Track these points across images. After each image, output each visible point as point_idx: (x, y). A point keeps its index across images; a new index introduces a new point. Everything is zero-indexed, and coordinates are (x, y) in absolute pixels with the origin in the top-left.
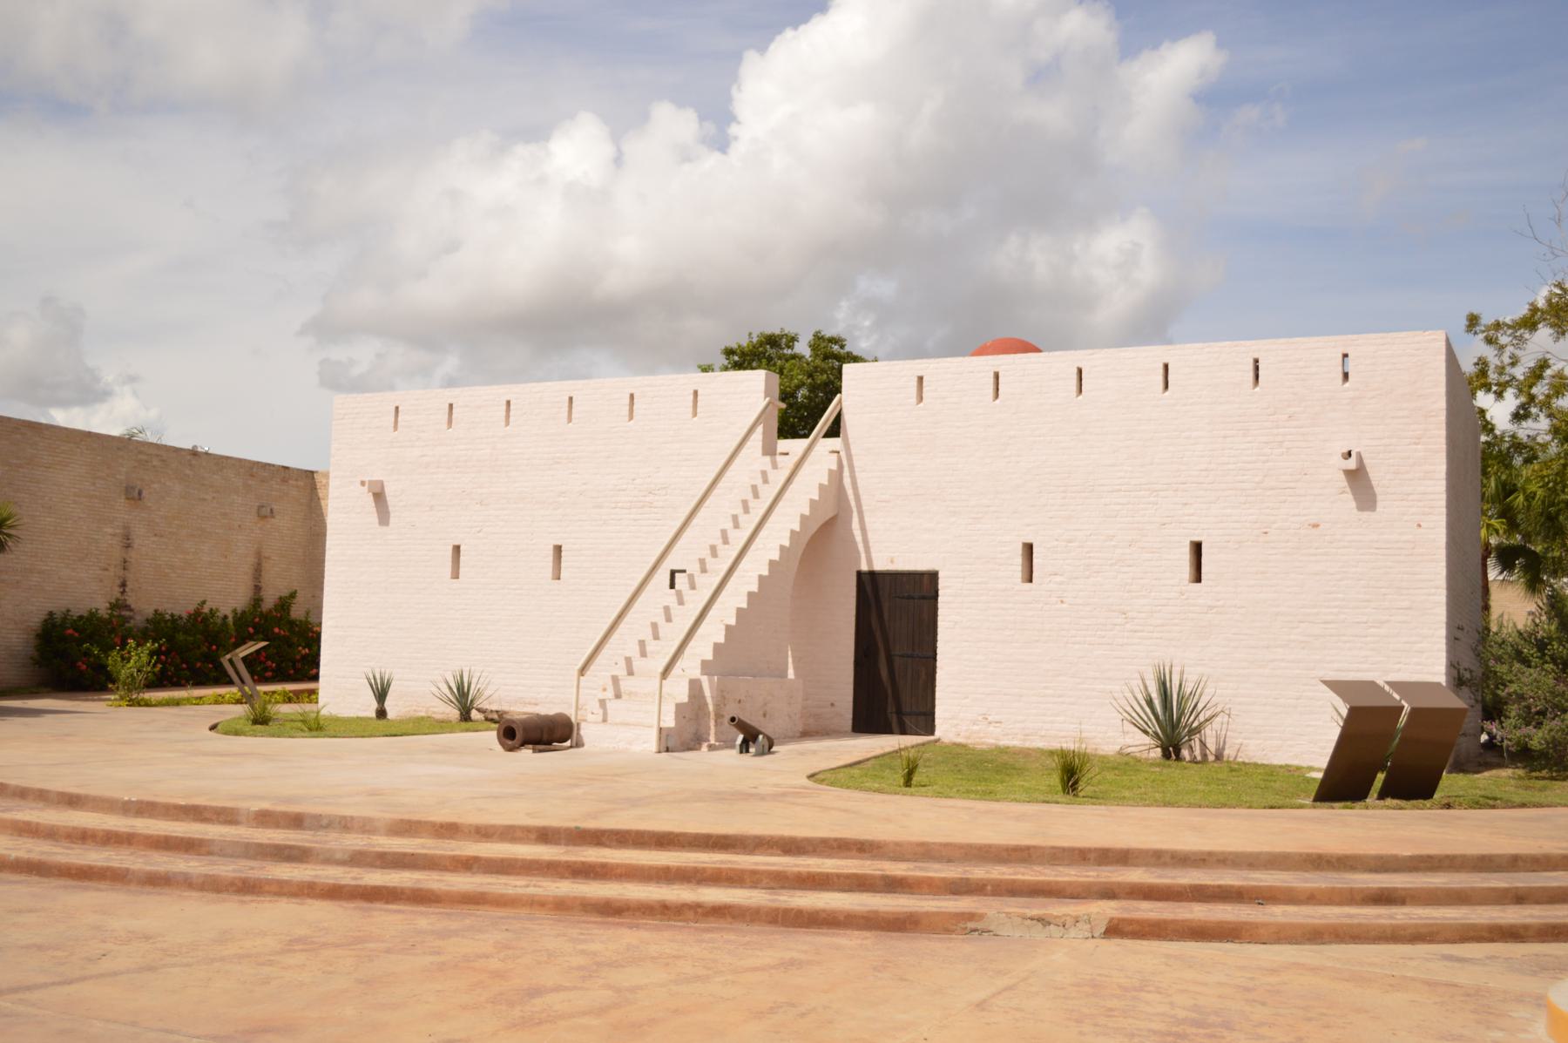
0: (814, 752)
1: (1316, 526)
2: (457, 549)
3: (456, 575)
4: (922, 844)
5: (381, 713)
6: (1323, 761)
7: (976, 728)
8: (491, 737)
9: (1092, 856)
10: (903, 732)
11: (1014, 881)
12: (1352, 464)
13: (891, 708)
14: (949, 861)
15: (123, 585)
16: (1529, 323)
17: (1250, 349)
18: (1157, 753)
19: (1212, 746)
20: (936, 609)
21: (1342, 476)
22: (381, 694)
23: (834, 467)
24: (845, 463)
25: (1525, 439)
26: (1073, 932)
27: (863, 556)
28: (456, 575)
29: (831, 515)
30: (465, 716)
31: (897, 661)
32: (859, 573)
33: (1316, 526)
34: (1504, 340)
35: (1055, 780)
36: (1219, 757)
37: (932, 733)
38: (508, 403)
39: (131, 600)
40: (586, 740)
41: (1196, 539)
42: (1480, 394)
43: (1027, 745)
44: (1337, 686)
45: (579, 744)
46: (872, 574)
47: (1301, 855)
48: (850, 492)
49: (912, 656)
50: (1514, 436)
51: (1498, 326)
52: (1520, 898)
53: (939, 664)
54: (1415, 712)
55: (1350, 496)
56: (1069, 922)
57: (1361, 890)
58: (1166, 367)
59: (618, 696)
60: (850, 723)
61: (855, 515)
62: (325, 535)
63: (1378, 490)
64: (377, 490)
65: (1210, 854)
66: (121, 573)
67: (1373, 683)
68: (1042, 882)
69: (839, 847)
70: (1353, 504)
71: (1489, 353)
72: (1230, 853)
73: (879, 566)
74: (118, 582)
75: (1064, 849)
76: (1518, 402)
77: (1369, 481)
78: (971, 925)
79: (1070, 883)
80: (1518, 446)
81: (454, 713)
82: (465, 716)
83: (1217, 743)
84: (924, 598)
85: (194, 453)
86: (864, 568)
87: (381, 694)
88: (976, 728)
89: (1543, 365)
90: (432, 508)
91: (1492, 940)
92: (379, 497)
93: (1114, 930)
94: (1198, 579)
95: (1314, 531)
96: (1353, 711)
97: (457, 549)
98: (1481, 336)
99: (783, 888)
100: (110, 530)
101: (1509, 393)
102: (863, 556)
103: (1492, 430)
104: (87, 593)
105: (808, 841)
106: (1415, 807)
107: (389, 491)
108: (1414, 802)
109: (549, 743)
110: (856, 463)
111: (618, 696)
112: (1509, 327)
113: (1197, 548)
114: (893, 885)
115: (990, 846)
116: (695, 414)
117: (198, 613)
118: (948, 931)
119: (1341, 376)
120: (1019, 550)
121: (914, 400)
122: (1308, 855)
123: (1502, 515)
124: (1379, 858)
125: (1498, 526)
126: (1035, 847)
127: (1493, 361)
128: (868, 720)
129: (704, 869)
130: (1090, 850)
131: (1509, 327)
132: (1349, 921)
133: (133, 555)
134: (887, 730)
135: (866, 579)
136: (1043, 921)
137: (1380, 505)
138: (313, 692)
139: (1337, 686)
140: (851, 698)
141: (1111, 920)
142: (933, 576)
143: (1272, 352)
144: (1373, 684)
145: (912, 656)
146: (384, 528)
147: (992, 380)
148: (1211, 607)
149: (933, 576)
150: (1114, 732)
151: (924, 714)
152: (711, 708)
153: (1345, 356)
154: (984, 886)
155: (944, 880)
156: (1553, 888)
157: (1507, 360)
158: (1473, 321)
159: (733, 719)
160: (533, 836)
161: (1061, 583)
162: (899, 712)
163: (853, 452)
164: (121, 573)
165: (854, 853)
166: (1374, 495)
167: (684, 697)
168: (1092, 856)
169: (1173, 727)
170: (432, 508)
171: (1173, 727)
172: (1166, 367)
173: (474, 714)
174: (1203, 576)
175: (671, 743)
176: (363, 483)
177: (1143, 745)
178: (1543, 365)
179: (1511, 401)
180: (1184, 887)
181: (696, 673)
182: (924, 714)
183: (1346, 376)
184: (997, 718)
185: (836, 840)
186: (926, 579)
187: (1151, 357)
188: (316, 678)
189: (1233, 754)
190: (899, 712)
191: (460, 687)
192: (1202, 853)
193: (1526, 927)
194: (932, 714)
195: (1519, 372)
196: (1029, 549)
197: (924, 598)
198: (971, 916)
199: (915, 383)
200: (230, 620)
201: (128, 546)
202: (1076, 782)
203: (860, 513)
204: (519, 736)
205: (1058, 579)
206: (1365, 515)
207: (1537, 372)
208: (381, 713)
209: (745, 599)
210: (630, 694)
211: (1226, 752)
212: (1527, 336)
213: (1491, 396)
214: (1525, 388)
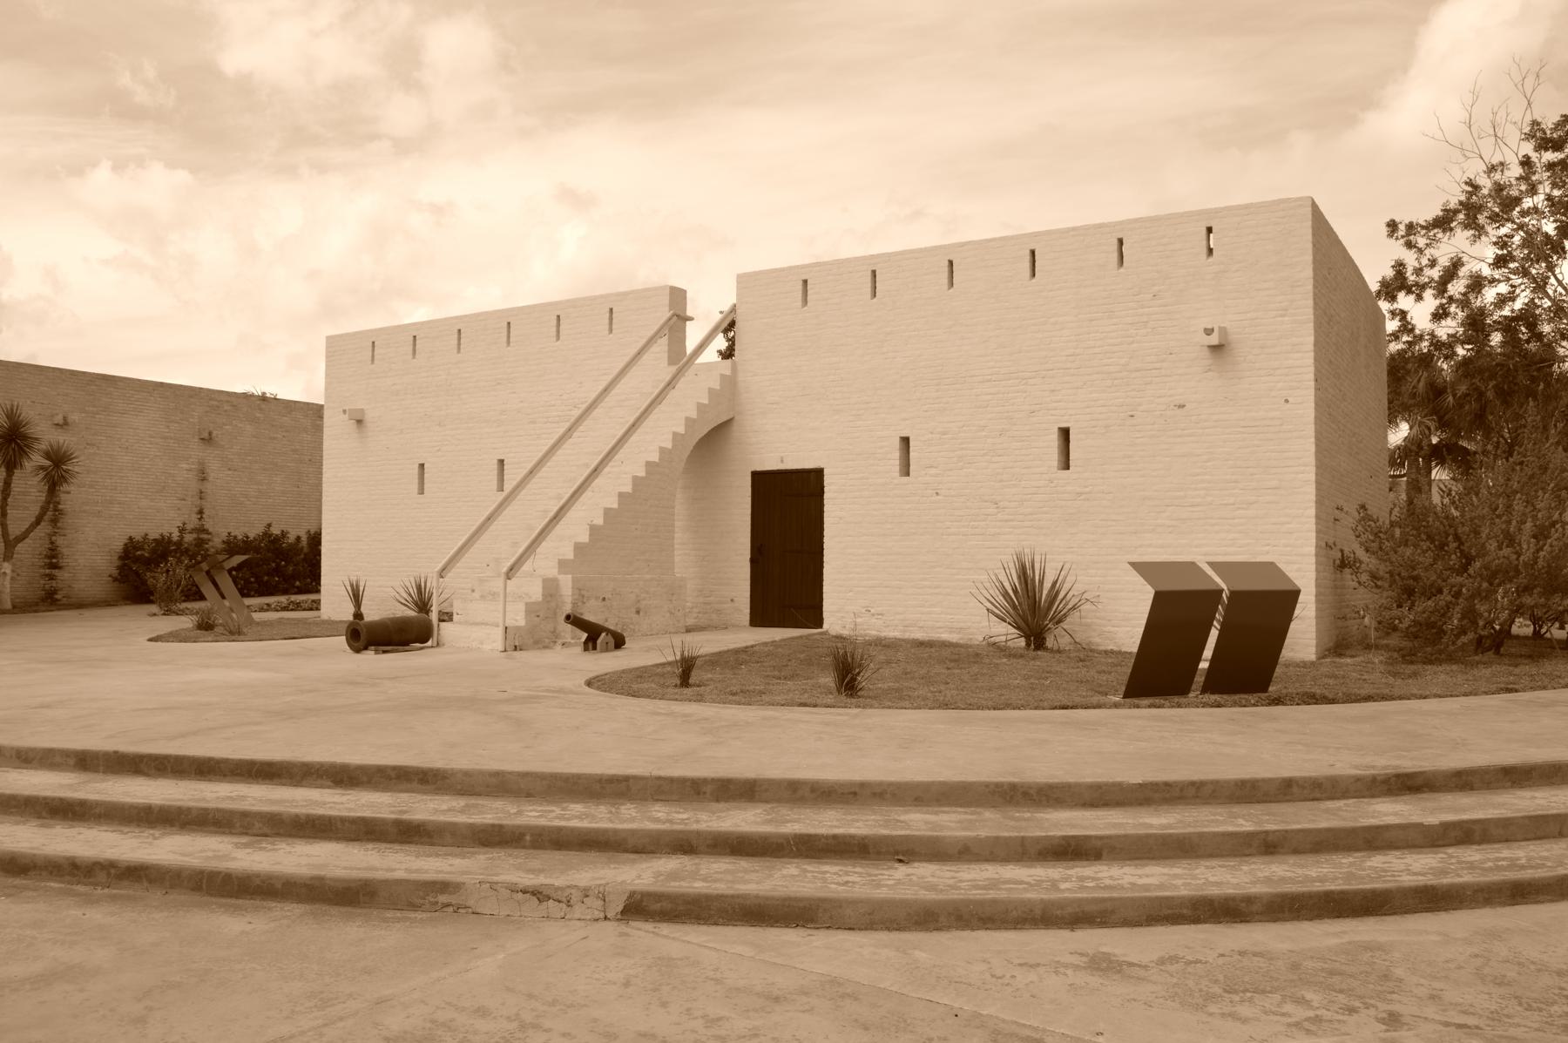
1: (1182, 406)
3: (421, 491)
4: (497, 774)
6: (1135, 650)
9: (708, 789)
11: (560, 829)
12: (1214, 340)
14: (529, 795)
15: (201, 512)
16: (1443, 222)
18: (1022, 642)
20: (822, 505)
23: (728, 373)
25: (1445, 337)
26: (578, 911)
28: (421, 491)
33: (1182, 406)
34: (1422, 242)
35: (828, 680)
42: (1401, 295)
44: (1142, 568)
47: (987, 785)
50: (1432, 334)
51: (1411, 227)
52: (1269, 845)
54: (1234, 595)
56: (576, 896)
57: (1038, 840)
58: (1033, 253)
65: (863, 785)
67: (1193, 563)
68: (597, 831)
69: (398, 777)
71: (1410, 259)
72: (891, 784)
75: (671, 780)
76: (1438, 302)
78: (443, 899)
79: (633, 832)
80: (1437, 344)
85: (263, 398)
89: (1456, 264)
91: (1196, 920)
93: (638, 908)
94: (1066, 466)
95: (1179, 412)
96: (1160, 598)
98: (1402, 241)
99: (278, 835)
101: (1428, 294)
103: (1412, 330)
104: (161, 517)
105: (363, 769)
106: (1235, 704)
108: (1236, 697)
109: (406, 643)
112: (1423, 227)
113: (1065, 433)
114: (408, 833)
115: (579, 776)
117: (266, 534)
118: (414, 907)
119: (1205, 250)
120: (897, 443)
121: (800, 304)
122: (997, 785)
123: (1434, 412)
124: (1097, 787)
125: (1429, 423)
126: (636, 778)
127: (1410, 259)
129: (189, 809)
130: (705, 781)
131: (1423, 227)
132: (992, 894)
133: (208, 487)
136: (539, 894)
138: (318, 602)
139: (1142, 568)
141: (632, 894)
142: (819, 473)
144: (1192, 565)
147: (869, 278)
149: (819, 473)
150: (974, 619)
153: (1210, 230)
154: (522, 835)
155: (471, 826)
156: (1319, 831)
157: (1425, 262)
158: (1392, 226)
159: (568, 617)
160: (72, 762)
165: (415, 785)
167: (536, 592)
168: (708, 789)
169: (1034, 611)
171: (1034, 611)
172: (1033, 253)
175: (516, 643)
177: (1004, 632)
178: (1456, 264)
179: (1430, 302)
180: (786, 837)
181: (553, 572)
183: (1210, 251)
185: (394, 768)
188: (318, 591)
191: (419, 588)
192: (852, 784)
193: (1249, 900)
195: (1435, 273)
196: (906, 441)
198: (444, 887)
199: (800, 286)
200: (304, 539)
201: (204, 479)
202: (854, 679)
204: (363, 637)
205: (933, 471)
207: (1451, 272)
212: (1440, 235)
213: (1412, 297)
214: (1441, 287)
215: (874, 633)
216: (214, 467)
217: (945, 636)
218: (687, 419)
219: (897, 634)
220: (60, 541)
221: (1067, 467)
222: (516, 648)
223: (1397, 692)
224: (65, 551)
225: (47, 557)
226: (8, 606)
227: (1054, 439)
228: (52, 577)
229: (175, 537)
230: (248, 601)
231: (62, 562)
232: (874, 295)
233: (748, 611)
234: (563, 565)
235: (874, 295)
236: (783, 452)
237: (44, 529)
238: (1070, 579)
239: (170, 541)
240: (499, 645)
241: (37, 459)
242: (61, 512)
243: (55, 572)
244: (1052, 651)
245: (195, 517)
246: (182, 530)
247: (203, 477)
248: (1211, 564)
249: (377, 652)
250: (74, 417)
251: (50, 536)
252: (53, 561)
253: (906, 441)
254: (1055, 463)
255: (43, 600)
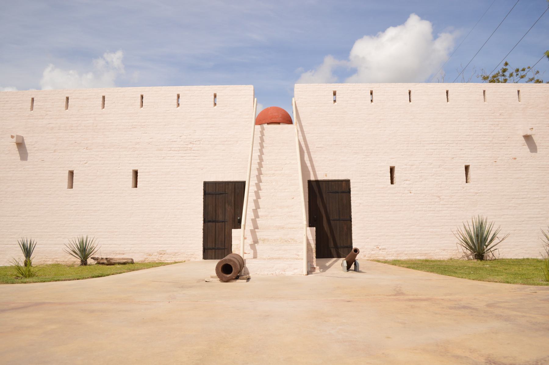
1: (515, 159)
2: (71, 173)
3: (71, 186)
5: (27, 263)
7: (373, 252)
13: (332, 244)
17: (139, 91)
21: (523, 139)
22: (28, 252)
28: (71, 186)
30: (84, 263)
33: (515, 159)
38: (104, 97)
43: (399, 258)
46: (317, 182)
55: (527, 147)
59: (255, 257)
62: (349, 192)
63: (537, 144)
64: (20, 141)
70: (528, 150)
73: (320, 177)
77: (533, 140)
81: (78, 261)
82: (84, 263)
84: (343, 192)
86: (312, 178)
87: (28, 252)
88: (373, 252)
90: (55, 151)
92: (20, 145)
95: (514, 161)
97: (71, 173)
107: (27, 142)
111: (255, 257)
135: (314, 185)
137: (538, 150)
142: (348, 182)
143: (149, 92)
145: (339, 220)
146: (24, 162)
148: (477, 193)
149: (348, 182)
150: (453, 249)
151: (347, 247)
161: (409, 184)
166: (536, 146)
169: (479, 245)
170: (55, 151)
171: (479, 245)
173: (90, 261)
176: (12, 137)
182: (347, 247)
184: (384, 247)
186: (344, 184)
187: (405, 87)
197: (343, 192)
199: (101, 99)
205: (408, 182)
206: (533, 154)
208: (27, 263)
210: (264, 240)
223: (105, 273)
227: (67, 175)
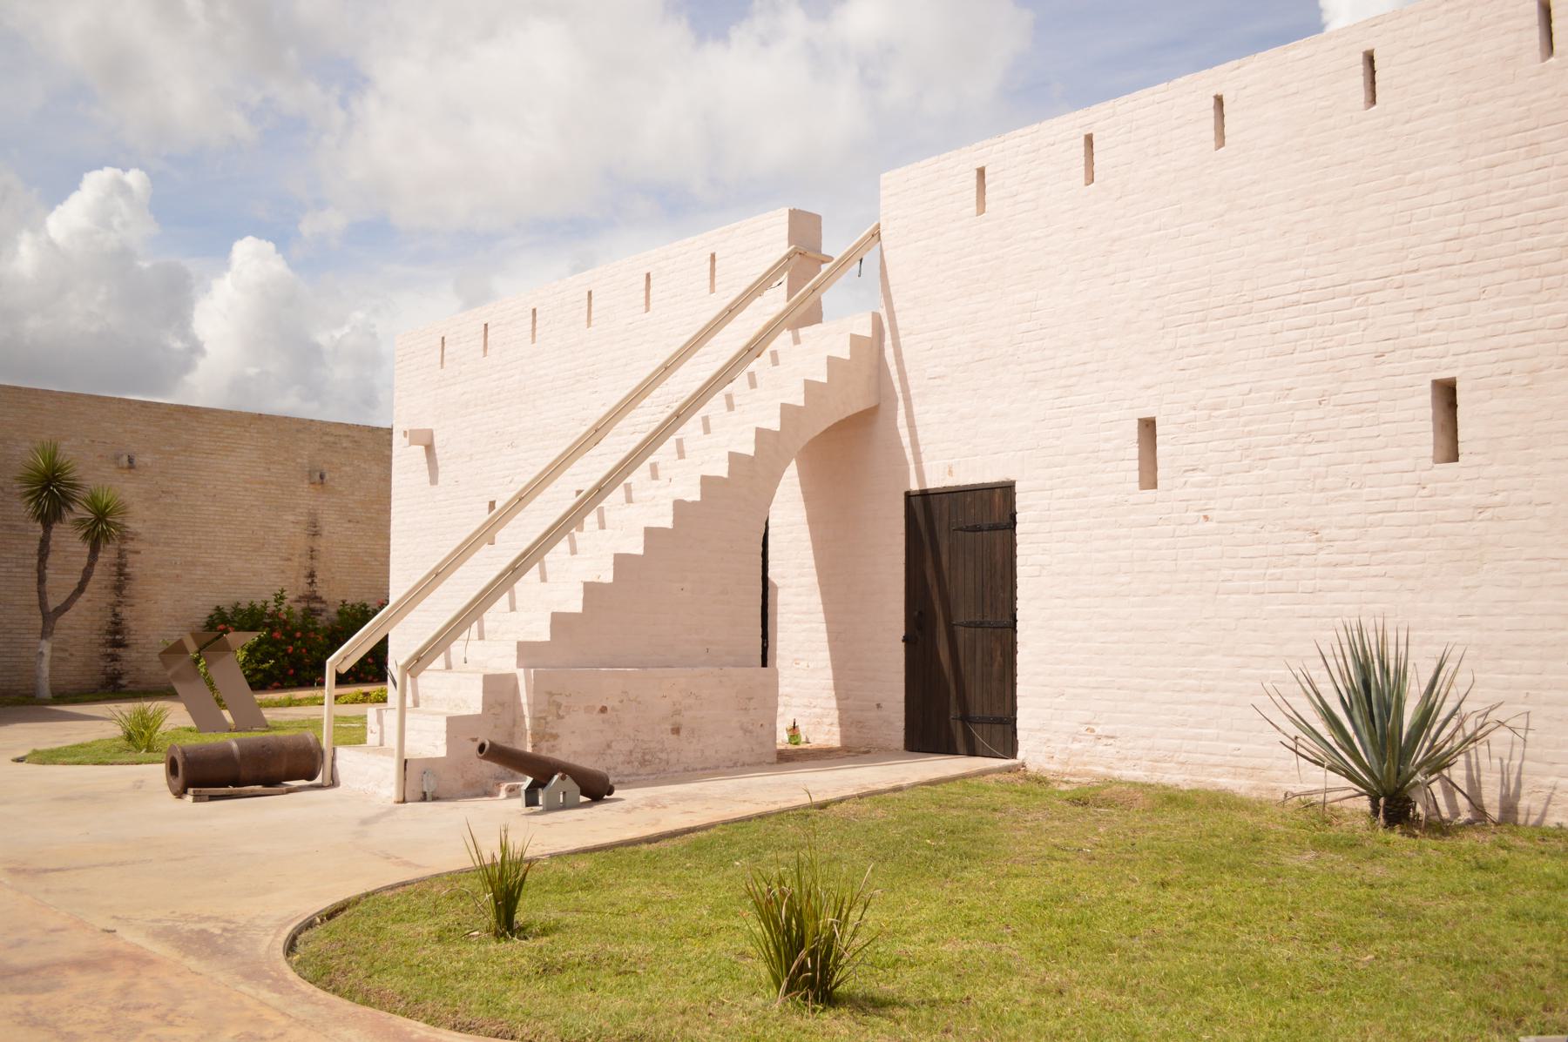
0: (693, 798)
8: (157, 772)
10: (972, 752)
13: (954, 713)
15: (312, 575)
19: (1491, 798)
24: (886, 325)
27: (912, 467)
29: (859, 406)
31: (963, 635)
32: (908, 495)
36: (1509, 809)
37: (1013, 755)
39: (322, 592)
40: (342, 774)
41: (1444, 375)
45: (333, 783)
46: (925, 494)
48: (893, 369)
49: (980, 625)
53: (1020, 637)
58: (1370, 59)
60: (901, 735)
61: (901, 404)
66: (308, 563)
73: (934, 482)
74: (305, 572)
83: (1504, 783)
86: (914, 486)
88: (1076, 746)
100: (291, 518)
102: (912, 467)
110: (900, 323)
116: (712, 290)
120: (1133, 428)
128: (929, 729)
133: (321, 544)
134: (948, 749)
140: (901, 696)
145: (980, 625)
148: (1482, 508)
151: (1000, 721)
152: (527, 721)
161: (1203, 485)
162: (966, 719)
163: (896, 307)
164: (308, 563)
172: (1370, 59)
174: (1461, 448)
181: (505, 662)
182: (1000, 721)
189: (1537, 807)
190: (966, 719)
191: (1364, 669)
194: (1012, 721)
196: (1148, 427)
203: (908, 400)
205: (1197, 477)
209: (641, 539)
211: (1523, 803)
215: (1101, 770)
216: (331, 522)
217: (1225, 782)
218: (784, 407)
219: (1138, 774)
220: (125, 612)
221: (1454, 456)
222: (424, 798)
224: (132, 625)
225: (109, 632)
226: (46, 692)
227: (1423, 405)
228: (115, 658)
229: (271, 607)
230: (261, 697)
231: (129, 639)
232: (1090, 179)
233: (902, 724)
234: (527, 651)
235: (1090, 179)
236: (945, 465)
237: (53, 603)
238: (1463, 678)
239: (262, 613)
240: (390, 791)
241: (80, 511)
242: (127, 577)
243: (120, 651)
244: (1440, 828)
245: (303, 581)
246: (280, 598)
247: (314, 531)
248: (789, 298)
249: (198, 798)
250: (143, 459)
251: (113, 606)
252: (116, 636)
253: (1148, 427)
254: (1429, 450)
255: (103, 687)
